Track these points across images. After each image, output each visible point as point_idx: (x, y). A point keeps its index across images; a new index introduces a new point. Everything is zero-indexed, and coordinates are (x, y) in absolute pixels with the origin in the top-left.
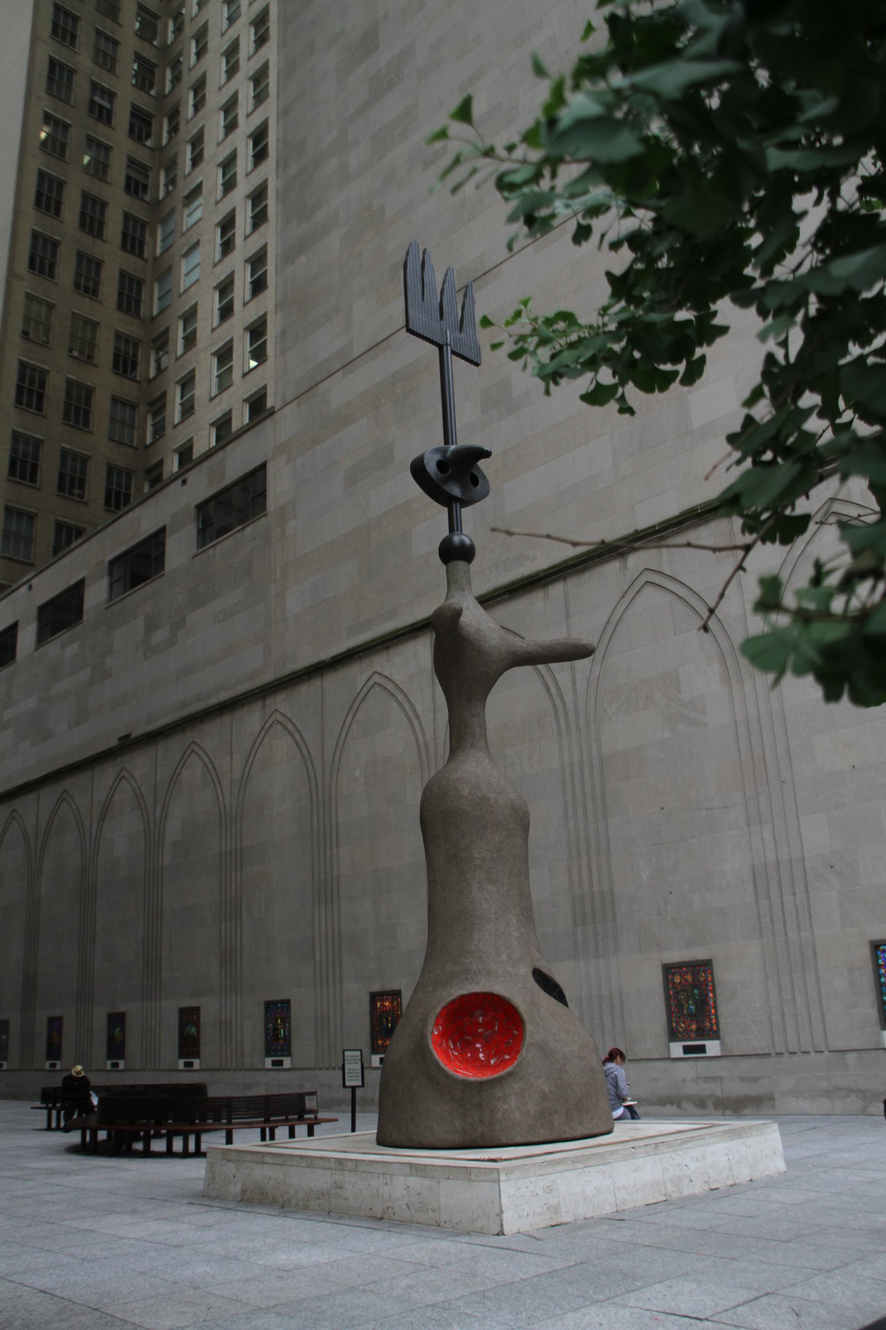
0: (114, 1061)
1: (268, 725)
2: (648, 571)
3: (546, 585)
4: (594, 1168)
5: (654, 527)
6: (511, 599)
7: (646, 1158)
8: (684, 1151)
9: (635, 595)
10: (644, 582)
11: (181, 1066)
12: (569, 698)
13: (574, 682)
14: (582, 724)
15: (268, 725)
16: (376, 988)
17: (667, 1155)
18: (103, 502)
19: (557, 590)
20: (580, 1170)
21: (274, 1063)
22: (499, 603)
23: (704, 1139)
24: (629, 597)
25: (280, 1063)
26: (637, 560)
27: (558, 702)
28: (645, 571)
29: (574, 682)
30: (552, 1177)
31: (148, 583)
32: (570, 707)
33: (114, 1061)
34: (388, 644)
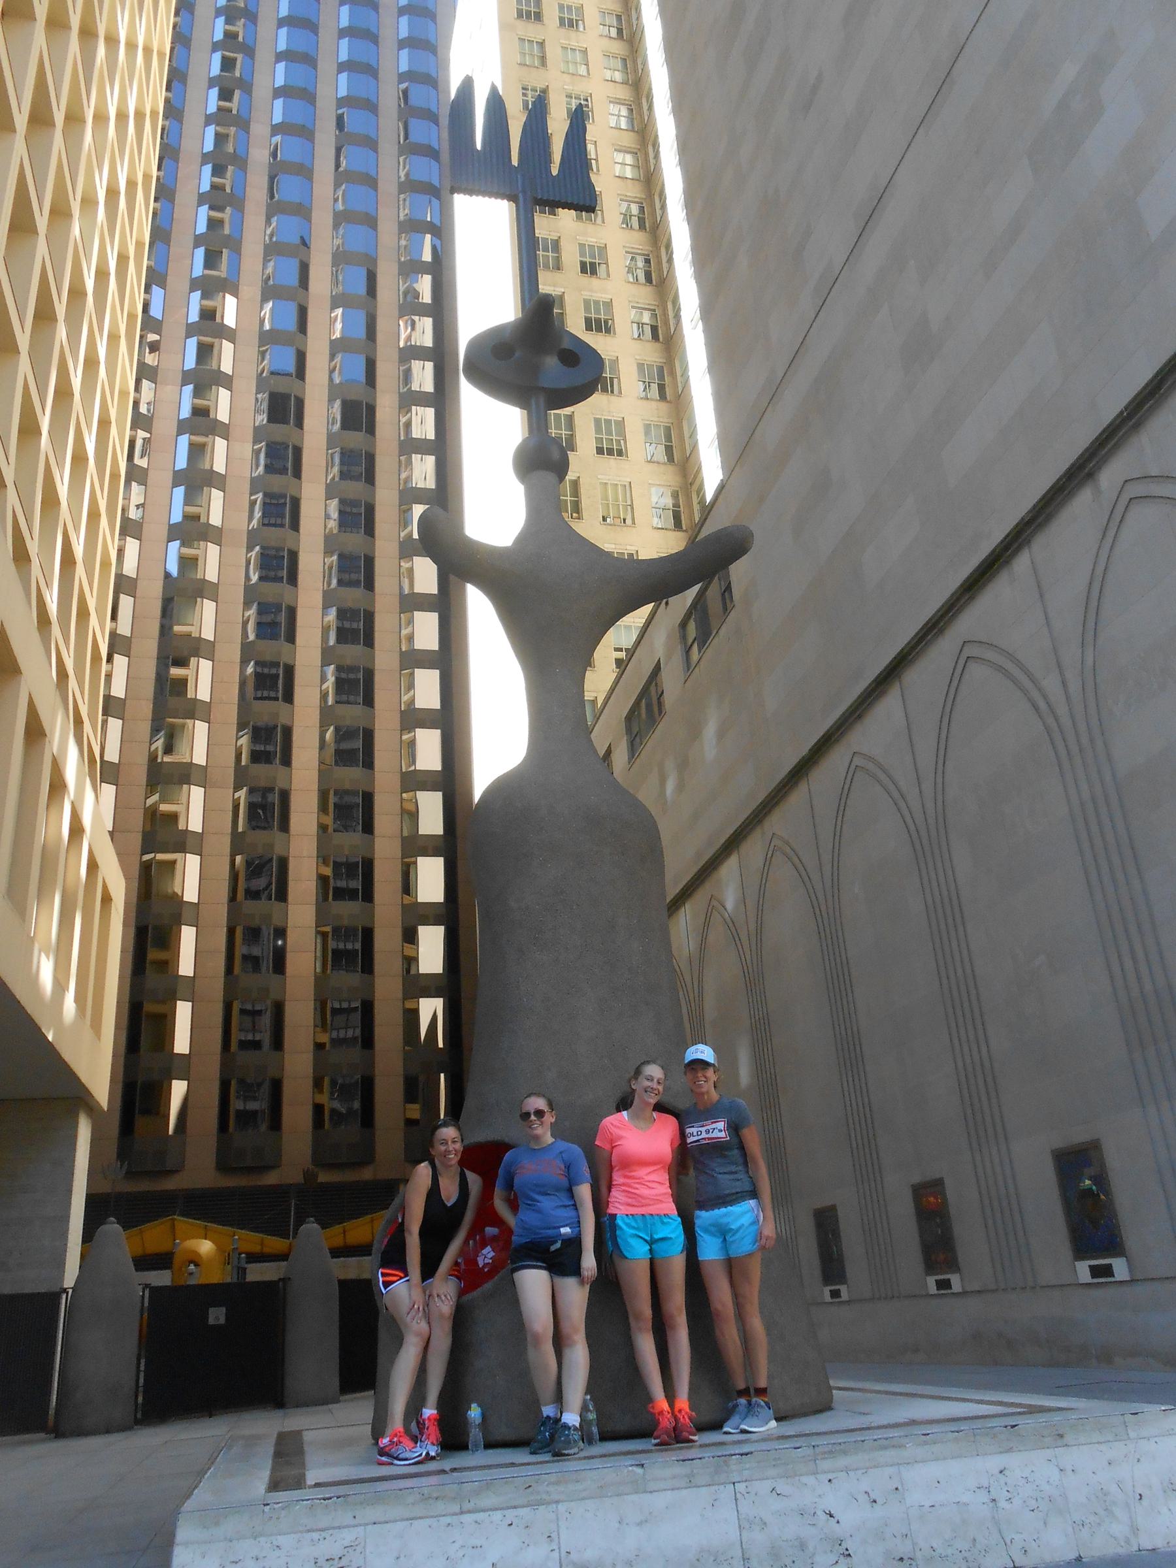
0: (833, 1288)
1: (769, 855)
2: (1131, 482)
3: (1007, 562)
4: (498, 1515)
5: (1121, 413)
6: (972, 598)
7: (684, 1492)
8: (824, 1478)
9: (1119, 527)
10: (1128, 500)
11: (932, 1288)
12: (1062, 710)
13: (1064, 683)
14: (1085, 741)
15: (769, 855)
16: (917, 1179)
17: (767, 1485)
18: (378, 678)
19: (1022, 563)
20: (448, 1520)
21: (1096, 1271)
22: (960, 611)
23: (900, 1446)
24: (1111, 533)
25: (1107, 1271)
26: (1110, 476)
27: (1050, 721)
28: (1127, 484)
29: (1064, 683)
30: (348, 1536)
31: (865, 708)
32: (1066, 721)
33: (833, 1288)
34: (858, 712)
